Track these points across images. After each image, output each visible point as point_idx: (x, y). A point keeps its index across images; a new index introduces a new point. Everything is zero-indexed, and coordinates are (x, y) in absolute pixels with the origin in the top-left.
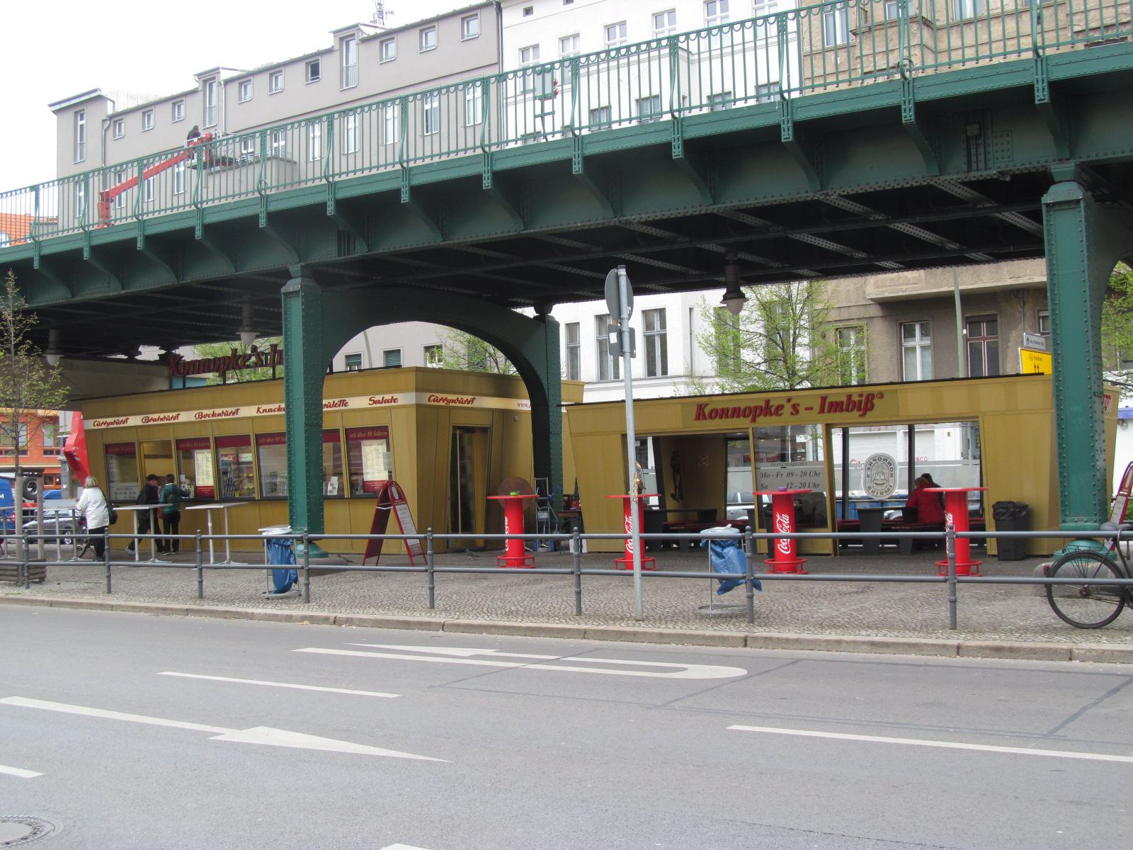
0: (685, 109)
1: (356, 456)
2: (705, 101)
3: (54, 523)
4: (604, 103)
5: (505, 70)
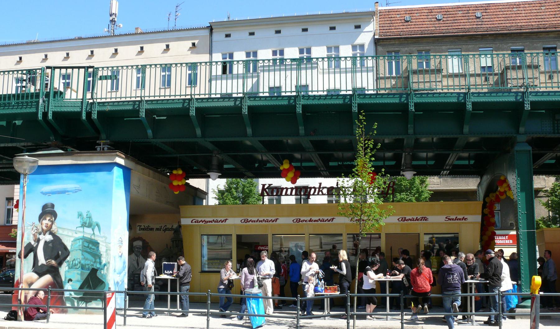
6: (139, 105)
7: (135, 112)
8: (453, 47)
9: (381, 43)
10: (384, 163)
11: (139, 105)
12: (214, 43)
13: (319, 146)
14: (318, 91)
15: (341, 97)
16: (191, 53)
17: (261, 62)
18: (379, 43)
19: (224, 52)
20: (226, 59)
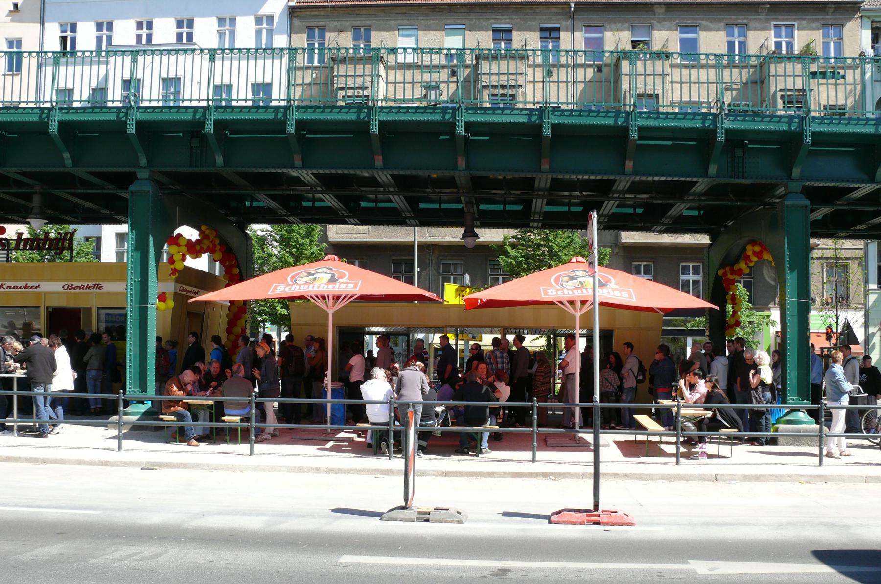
0: (40, 102)
1: (416, 347)
2: (161, 98)
3: (18, 397)
4: (226, 81)
5: (23, 50)
6: (48, 114)
7: (42, 126)
8: (405, 22)
9: (298, 13)
10: (504, 207)
11: (48, 114)
12: (46, 6)
13: (403, 183)
14: (191, 100)
15: (272, 110)
16: (12, 20)
17: (703, 57)
18: (295, 14)
19: (63, 22)
20: (66, 32)
